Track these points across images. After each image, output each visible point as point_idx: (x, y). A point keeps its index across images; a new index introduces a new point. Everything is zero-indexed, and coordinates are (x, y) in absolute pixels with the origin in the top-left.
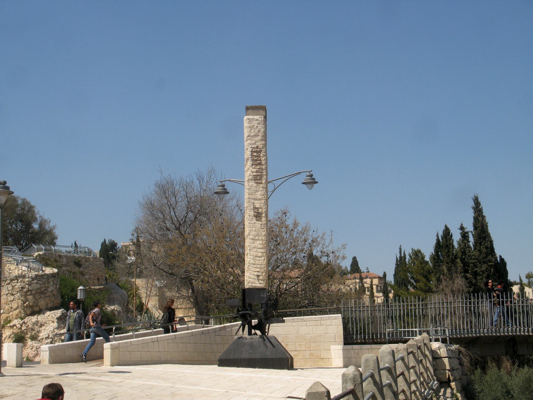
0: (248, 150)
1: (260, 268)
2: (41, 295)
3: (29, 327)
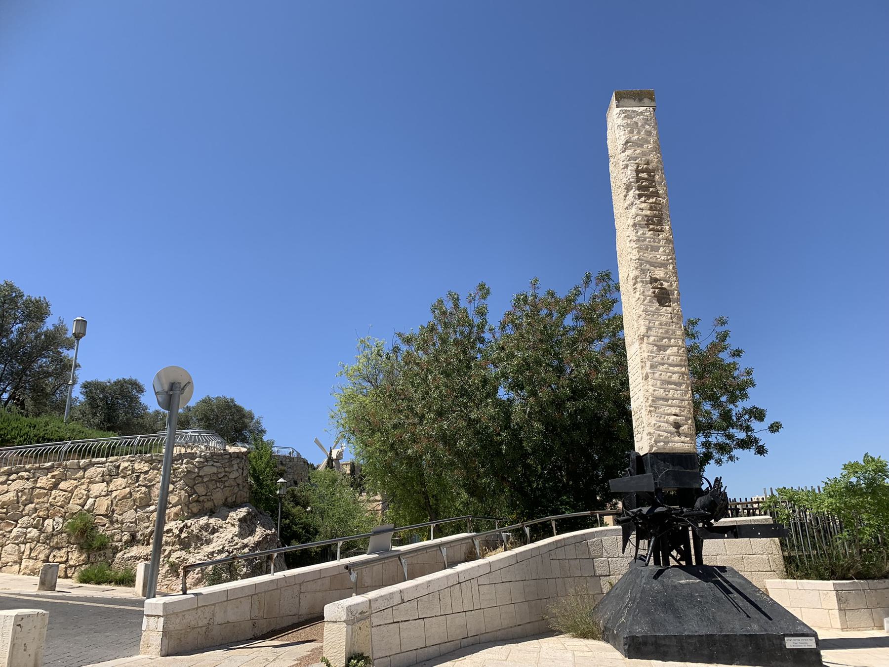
2: (218, 484)
3: (194, 533)
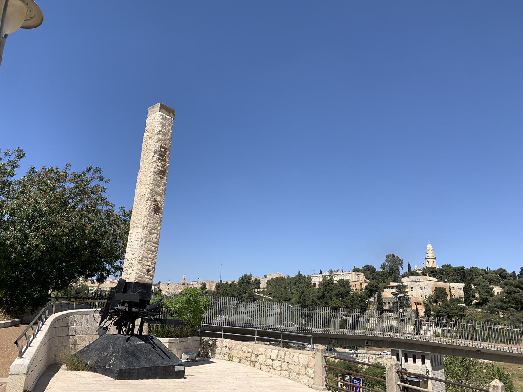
0: (158, 144)
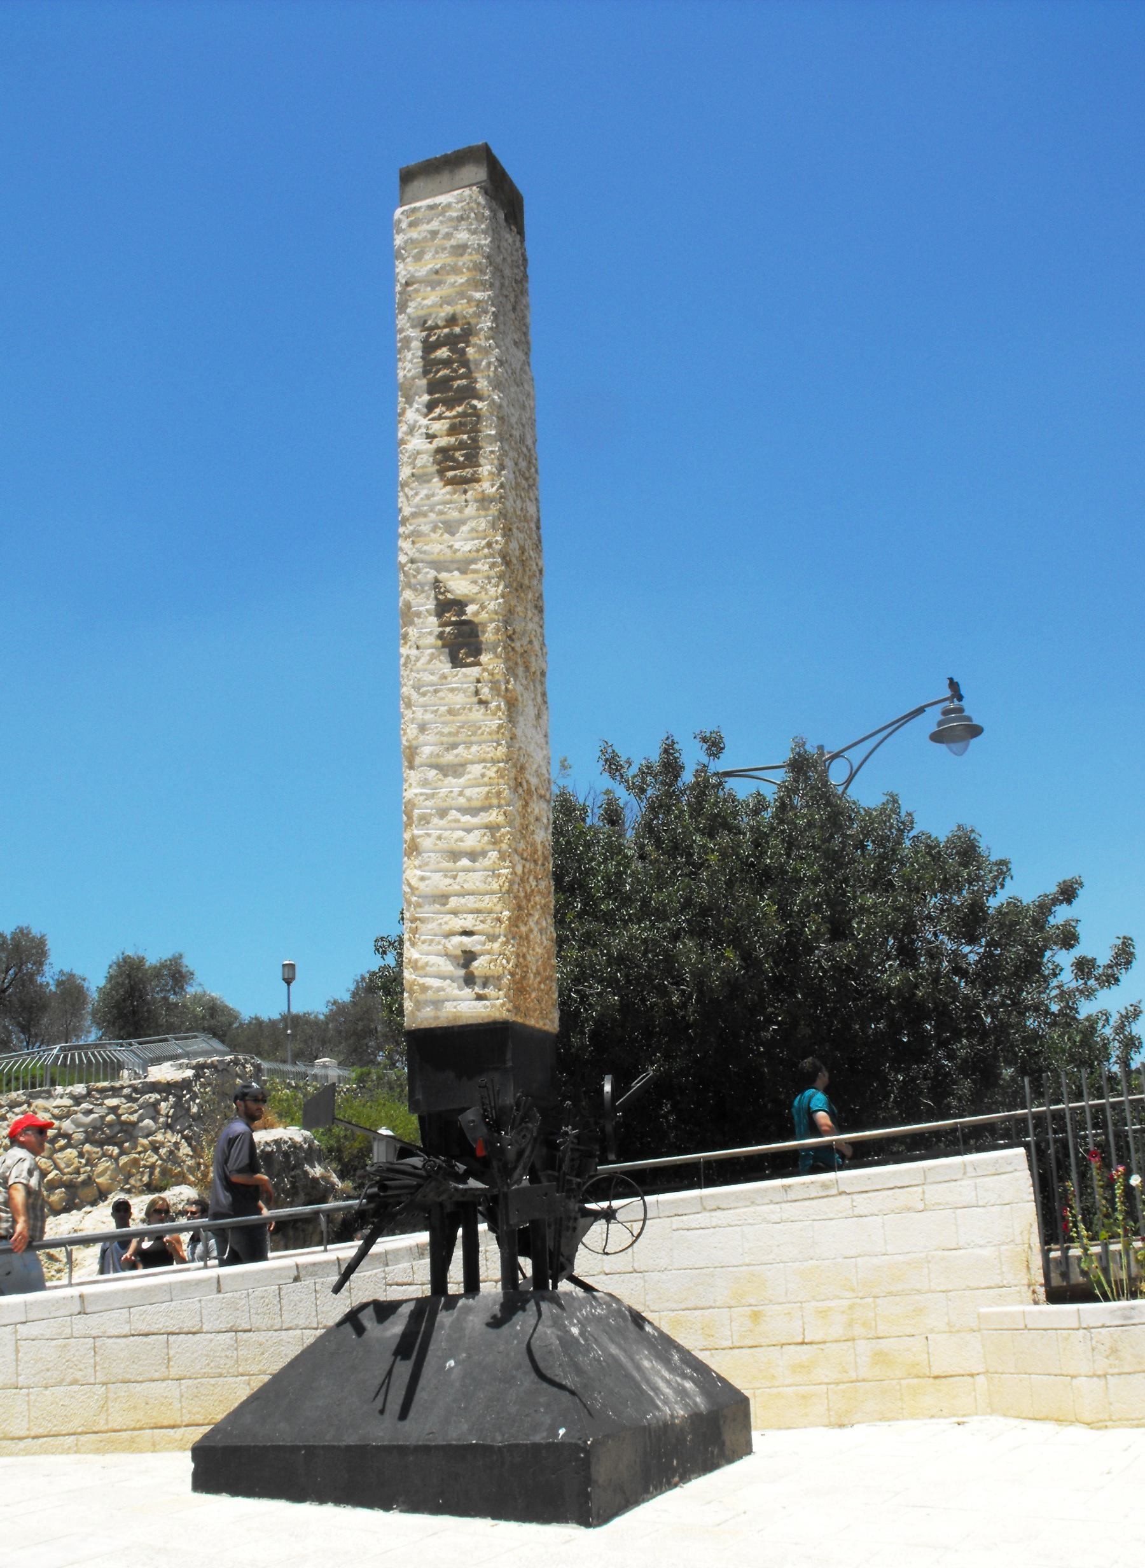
1: (478, 911)
